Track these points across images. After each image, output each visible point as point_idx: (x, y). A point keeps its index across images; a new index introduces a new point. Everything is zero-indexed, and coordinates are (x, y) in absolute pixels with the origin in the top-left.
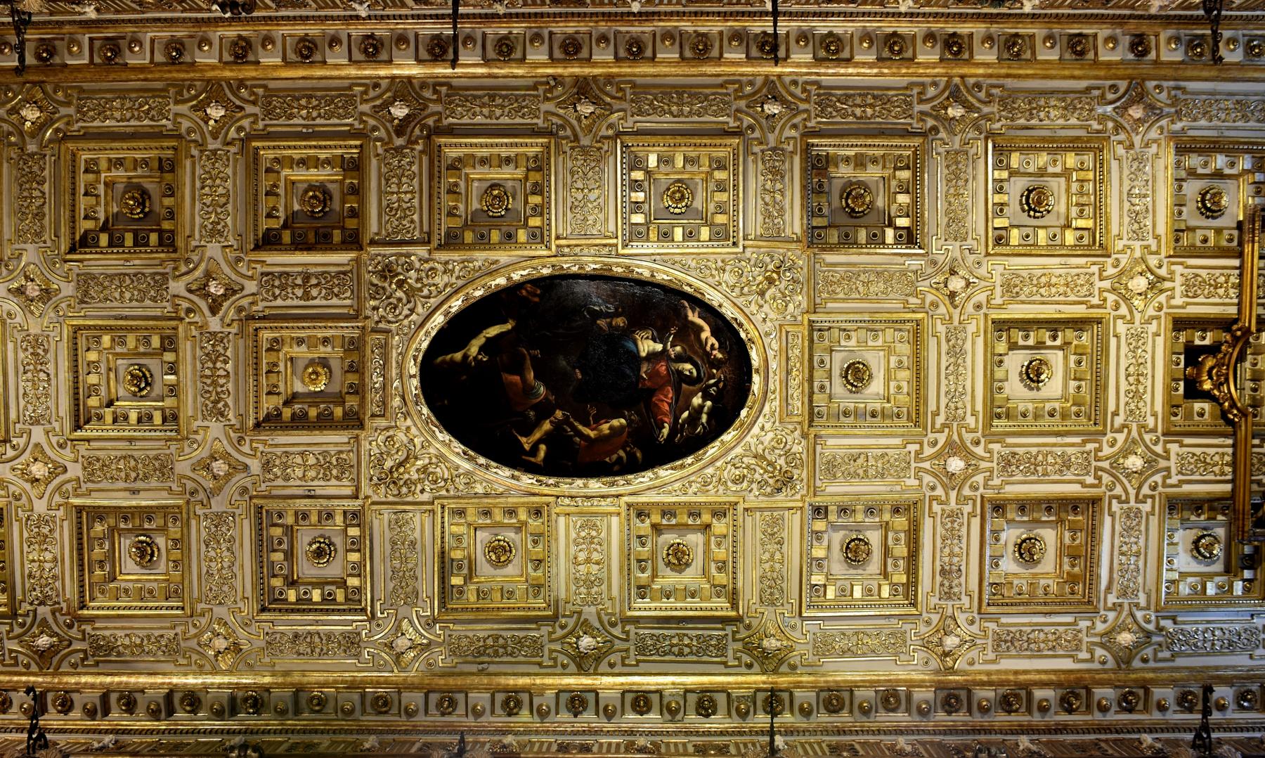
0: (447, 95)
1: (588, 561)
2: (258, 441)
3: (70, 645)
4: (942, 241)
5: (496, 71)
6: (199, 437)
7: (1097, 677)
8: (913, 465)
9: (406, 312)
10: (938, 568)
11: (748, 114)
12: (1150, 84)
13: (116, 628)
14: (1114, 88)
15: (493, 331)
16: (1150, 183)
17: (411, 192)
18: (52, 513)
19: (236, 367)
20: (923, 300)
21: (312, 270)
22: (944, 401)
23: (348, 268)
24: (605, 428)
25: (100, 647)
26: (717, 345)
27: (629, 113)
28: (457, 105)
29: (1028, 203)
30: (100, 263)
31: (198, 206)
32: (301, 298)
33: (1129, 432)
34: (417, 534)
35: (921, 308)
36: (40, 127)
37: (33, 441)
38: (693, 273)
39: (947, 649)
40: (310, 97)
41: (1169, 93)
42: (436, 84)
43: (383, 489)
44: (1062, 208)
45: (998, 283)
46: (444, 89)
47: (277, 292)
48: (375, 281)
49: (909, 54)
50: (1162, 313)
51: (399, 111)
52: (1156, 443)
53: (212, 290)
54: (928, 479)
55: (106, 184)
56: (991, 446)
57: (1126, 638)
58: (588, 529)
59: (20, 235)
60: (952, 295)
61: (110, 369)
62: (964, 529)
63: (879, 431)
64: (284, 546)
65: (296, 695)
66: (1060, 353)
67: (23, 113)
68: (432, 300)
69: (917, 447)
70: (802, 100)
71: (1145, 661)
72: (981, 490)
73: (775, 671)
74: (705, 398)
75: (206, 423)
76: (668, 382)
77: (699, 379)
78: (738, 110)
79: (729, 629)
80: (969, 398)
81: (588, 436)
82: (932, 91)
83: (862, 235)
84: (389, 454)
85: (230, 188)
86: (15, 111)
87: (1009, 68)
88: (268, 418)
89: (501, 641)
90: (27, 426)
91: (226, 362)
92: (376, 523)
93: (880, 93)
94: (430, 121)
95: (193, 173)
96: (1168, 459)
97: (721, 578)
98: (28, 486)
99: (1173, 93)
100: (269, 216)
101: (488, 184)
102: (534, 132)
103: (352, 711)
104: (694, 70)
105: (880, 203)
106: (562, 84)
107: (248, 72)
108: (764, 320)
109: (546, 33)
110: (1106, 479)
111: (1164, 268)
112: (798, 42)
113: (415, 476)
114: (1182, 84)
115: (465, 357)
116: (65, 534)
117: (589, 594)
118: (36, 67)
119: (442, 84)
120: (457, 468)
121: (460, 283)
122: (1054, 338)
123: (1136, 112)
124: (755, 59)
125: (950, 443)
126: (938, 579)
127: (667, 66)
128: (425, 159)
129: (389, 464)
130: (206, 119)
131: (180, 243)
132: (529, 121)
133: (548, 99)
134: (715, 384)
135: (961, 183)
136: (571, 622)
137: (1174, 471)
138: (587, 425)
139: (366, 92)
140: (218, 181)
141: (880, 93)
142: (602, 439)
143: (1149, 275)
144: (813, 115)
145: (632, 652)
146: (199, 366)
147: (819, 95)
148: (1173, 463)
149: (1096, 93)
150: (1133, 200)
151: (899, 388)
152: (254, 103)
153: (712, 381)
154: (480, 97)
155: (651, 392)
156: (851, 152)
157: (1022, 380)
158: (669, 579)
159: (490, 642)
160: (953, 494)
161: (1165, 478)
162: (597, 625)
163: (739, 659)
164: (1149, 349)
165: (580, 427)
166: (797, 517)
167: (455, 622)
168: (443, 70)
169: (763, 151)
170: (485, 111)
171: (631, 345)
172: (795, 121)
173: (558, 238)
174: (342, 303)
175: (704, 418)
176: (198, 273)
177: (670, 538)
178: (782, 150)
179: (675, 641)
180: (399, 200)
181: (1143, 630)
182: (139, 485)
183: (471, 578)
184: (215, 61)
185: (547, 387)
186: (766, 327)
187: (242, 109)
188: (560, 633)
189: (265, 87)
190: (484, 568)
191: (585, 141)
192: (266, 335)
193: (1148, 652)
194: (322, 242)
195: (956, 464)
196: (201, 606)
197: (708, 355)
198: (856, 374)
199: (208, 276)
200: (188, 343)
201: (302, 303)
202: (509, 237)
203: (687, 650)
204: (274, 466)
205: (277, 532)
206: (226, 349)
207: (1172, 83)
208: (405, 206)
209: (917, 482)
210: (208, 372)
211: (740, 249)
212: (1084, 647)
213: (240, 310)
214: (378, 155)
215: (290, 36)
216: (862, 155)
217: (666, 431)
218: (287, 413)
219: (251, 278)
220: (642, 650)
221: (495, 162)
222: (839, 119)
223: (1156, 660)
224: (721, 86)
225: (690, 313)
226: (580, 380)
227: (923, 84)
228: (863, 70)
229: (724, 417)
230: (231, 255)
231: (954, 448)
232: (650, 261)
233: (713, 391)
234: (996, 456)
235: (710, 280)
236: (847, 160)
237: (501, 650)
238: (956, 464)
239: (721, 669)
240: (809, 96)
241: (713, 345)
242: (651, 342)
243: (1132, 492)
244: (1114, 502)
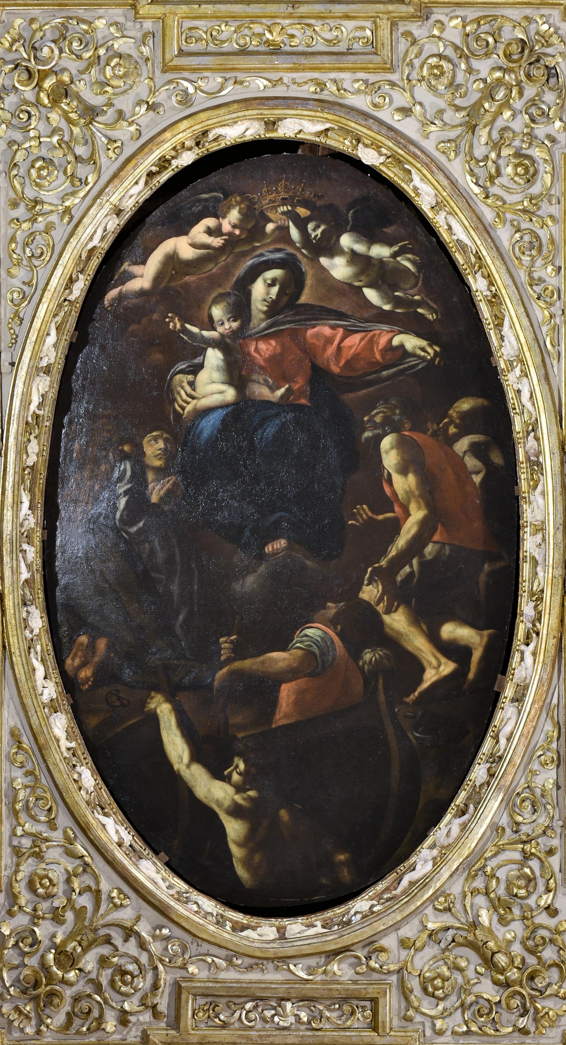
9: (131, 947)
24: (404, 484)
26: (210, 222)
38: (43, 274)
48: (60, 1018)
68: (104, 886)
77: (289, 264)
108: (152, 107)
115: (236, 811)
121: (63, 820)
129: (488, 990)
134: (301, 224)
138: (395, 527)
153: (294, 233)
155: (318, 374)
165: (401, 542)
171: (209, 425)
175: (380, 251)
185: (306, 621)
197: (232, 241)
217: (411, 342)
225: (135, 285)
229: (381, 205)
233: (316, 231)
241: (209, 232)
242: (203, 376)
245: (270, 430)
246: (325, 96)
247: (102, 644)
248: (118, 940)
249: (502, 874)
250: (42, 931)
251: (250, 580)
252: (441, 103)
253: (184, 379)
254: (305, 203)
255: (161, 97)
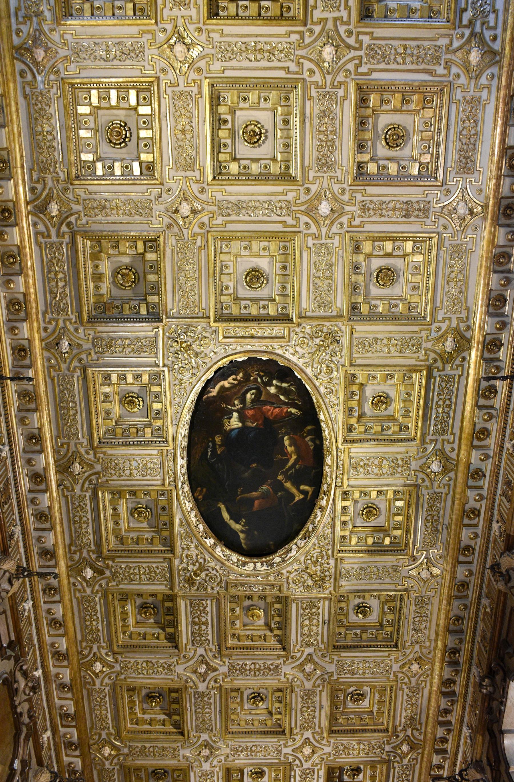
0: (76, 546)
1: (380, 467)
2: (294, 649)
3: (408, 736)
4: (153, 219)
5: (58, 520)
6: (291, 677)
7: (504, 83)
8: (323, 241)
9: (214, 572)
10: (404, 219)
11: (70, 363)
12: (16, 41)
13: (401, 716)
14: (22, 74)
15: (226, 516)
16: (97, 41)
17: (139, 568)
18: (332, 745)
19: (249, 659)
20: (198, 234)
21: (190, 620)
22: (275, 218)
23: (188, 602)
24: (290, 449)
25: (411, 723)
26: (234, 377)
27: (77, 441)
28: (82, 541)
29: (120, 144)
30: (190, 720)
31: (154, 676)
32: (207, 627)
33: (303, 57)
34: (356, 566)
35: (205, 237)
36: (114, 747)
37: (291, 752)
38: (184, 401)
39: (467, 212)
40: (85, 620)
41: (21, 23)
42: (69, 552)
43: (327, 585)
44: (122, 112)
45: (183, 173)
46: (73, 548)
47: (203, 638)
48: (195, 588)
49: (15, 249)
50: (204, 28)
51: (89, 573)
52: (311, 31)
53: (203, 671)
54: (335, 229)
55: (144, 713)
56: (311, 179)
57: (474, 57)
58: (361, 473)
59: (175, 756)
60: (194, 211)
61: (250, 713)
62: (375, 199)
63: (297, 269)
64: (359, 632)
65: (450, 632)
66: (238, 113)
67: (106, 755)
68: (207, 557)
69: (310, 238)
70: (57, 325)
71: (453, 450)
72: (345, 186)
73: (469, 341)
74: (271, 385)
75: (283, 674)
76: (260, 409)
77: (258, 389)
78: (69, 369)
79: (436, 373)
80: (273, 198)
81: (296, 460)
82: (41, 227)
83: (152, 278)
84: (304, 582)
85: (142, 660)
86: (97, 675)
87: (16, 167)
88: (280, 641)
89: (429, 518)
90: (283, 755)
91: (246, 665)
92: (346, 588)
93: (46, 267)
94: (93, 556)
95: (135, 678)
96: (327, 19)
97: (398, 375)
98: (316, 755)
99: (21, 19)
100: (158, 638)
101: (131, 518)
102: (95, 496)
103: (466, 606)
104: (44, 399)
105: (127, 260)
106: (62, 480)
107: (73, 652)
108: (215, 353)
109: (31, 496)
110: (341, 78)
111: (166, 26)
112: (16, 334)
113: (319, 567)
114: (12, 10)
115: (242, 532)
116: (344, 740)
117: (402, 467)
118: (80, 750)
119: (70, 550)
120: (314, 544)
121: (195, 541)
122: (226, 122)
123: (40, 54)
124: (31, 361)
125: (308, 213)
126: (412, 219)
127: (52, 499)
128: (117, 560)
129: (310, 582)
130: (102, 671)
131: (176, 686)
132: (88, 501)
133: (73, 490)
134: (261, 377)
135: (108, 206)
136: (421, 475)
137: (336, 14)
138: (288, 460)
139: (79, 591)
140: (139, 666)
141: (46, 267)
142: (298, 451)
143: (172, 42)
144: (67, 317)
145: (445, 437)
146: (248, 677)
147: (52, 313)
148: (330, 15)
149: (28, 89)
150: (112, 57)
151: (265, 249)
152: (91, 648)
153: (259, 380)
154: (75, 528)
155: (266, 420)
156: (91, 285)
157: (260, 146)
158: (396, 408)
159: (429, 524)
160: (347, 208)
161: (343, 23)
162: (424, 460)
163: (457, 366)
164: (233, 40)
165: (289, 464)
166: (358, 328)
167: (414, 545)
168: (60, 551)
169: (96, 353)
170: (84, 526)
171: (234, 433)
172: (72, 329)
173: (163, 484)
174: (210, 606)
175: (285, 385)
176: (194, 677)
177: (368, 408)
178: (94, 339)
179: (440, 410)
180: (144, 574)
181: (468, 41)
182: (317, 705)
183: (386, 531)
184: (60, 606)
186: (221, 347)
187: (95, 654)
188: (427, 483)
189: (81, 642)
190: (381, 521)
191: (98, 468)
192: (230, 642)
193: (488, 35)
194: (172, 612)
195: (324, 208)
196: (391, 677)
197: (240, 382)
198: (255, 276)
199: (195, 672)
200: (235, 682)
201: (210, 626)
202: (158, 397)
203: (447, 402)
204: (309, 641)
205: (349, 637)
206: (238, 664)
207: (13, 20)
208: (148, 571)
209: (337, 238)
210: (252, 673)
211: (166, 369)
212: (478, 95)
213: (214, 657)
214: (117, 585)
215: (48, 632)
216: (92, 278)
217: (293, 410)
218: (277, 632)
219: (195, 651)
220: (444, 432)
221: (117, 517)
222: (68, 298)
223: (495, 28)
224: (53, 380)
225: (212, 394)
226: (256, 456)
227: (36, 234)
228: (31, 281)
229: (285, 373)
230: (183, 660)
231: (311, 211)
232: (179, 429)
233: (266, 379)
234: (319, 174)
235: (188, 389)
236: (97, 288)
237: (435, 518)
238: (324, 208)
239: (463, 378)
240: (54, 319)
241: (234, 379)
242: (232, 420)
243: (353, 53)
244: (360, 70)
245: (252, 435)
246: (269, 350)
247: (204, 490)
248: (211, 570)
249: (315, 555)
250: (190, 568)
251: (246, 474)
252: (304, 351)
253: (227, 421)
254: (262, 372)
255: (218, 350)
